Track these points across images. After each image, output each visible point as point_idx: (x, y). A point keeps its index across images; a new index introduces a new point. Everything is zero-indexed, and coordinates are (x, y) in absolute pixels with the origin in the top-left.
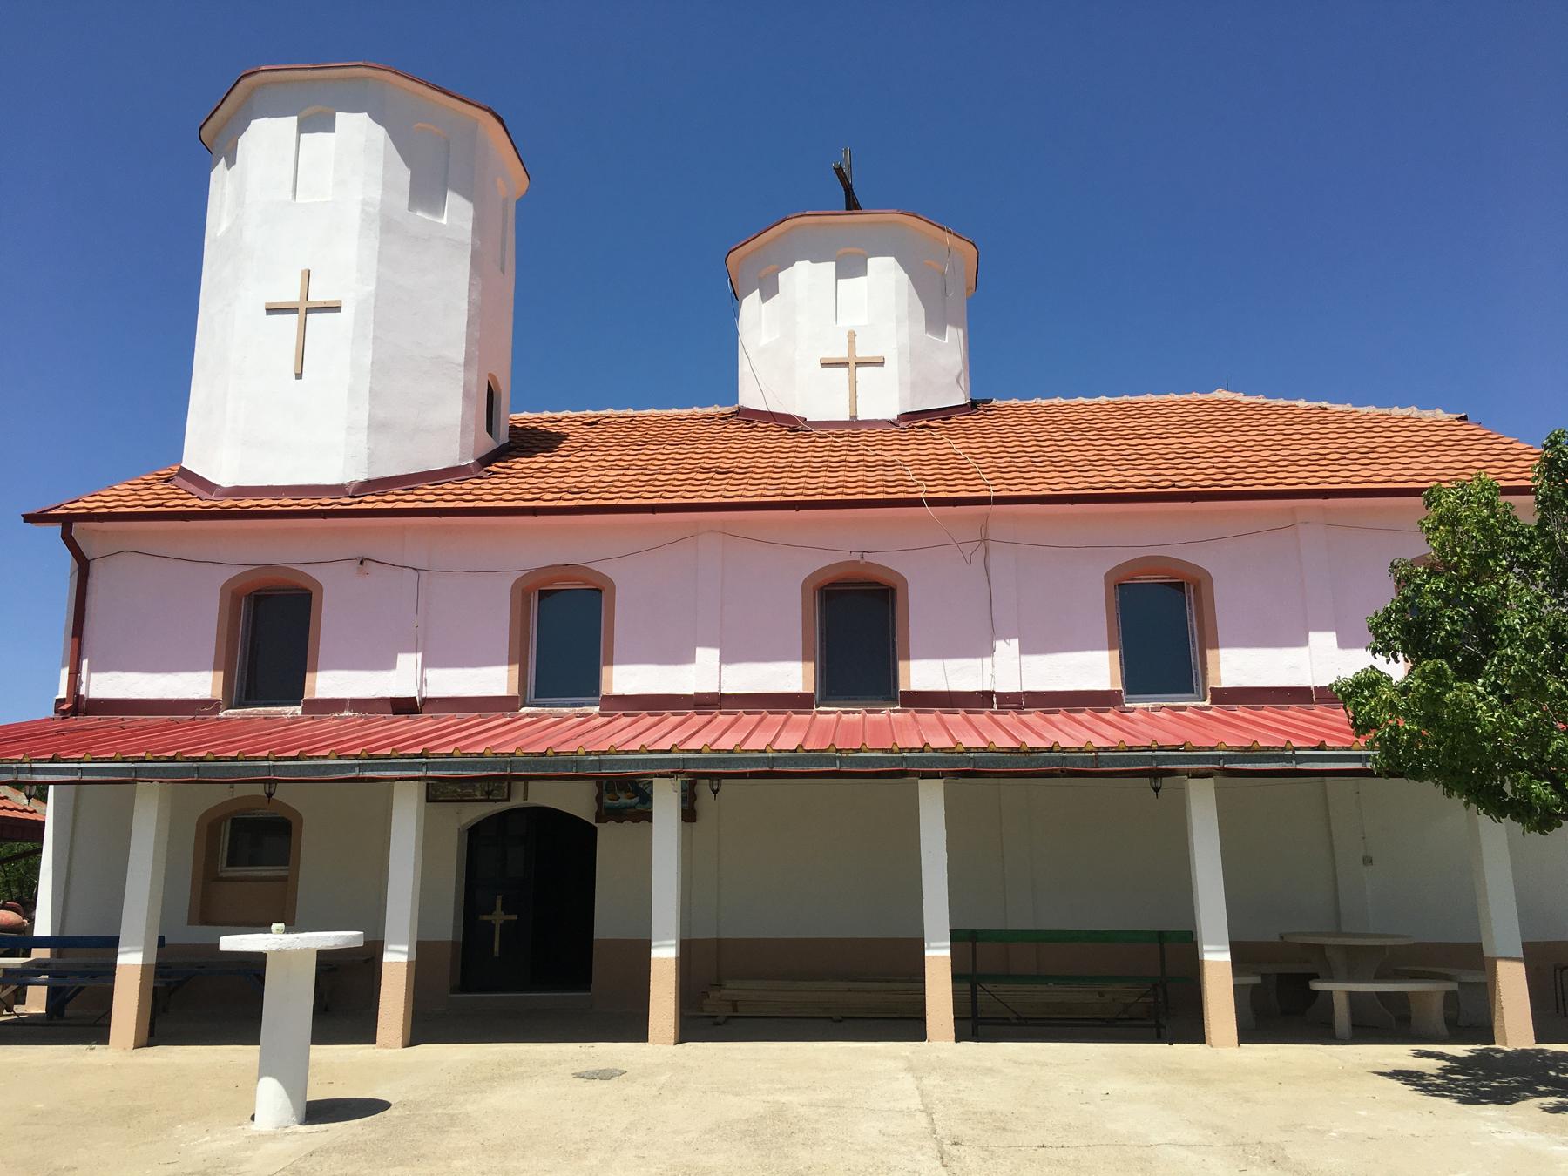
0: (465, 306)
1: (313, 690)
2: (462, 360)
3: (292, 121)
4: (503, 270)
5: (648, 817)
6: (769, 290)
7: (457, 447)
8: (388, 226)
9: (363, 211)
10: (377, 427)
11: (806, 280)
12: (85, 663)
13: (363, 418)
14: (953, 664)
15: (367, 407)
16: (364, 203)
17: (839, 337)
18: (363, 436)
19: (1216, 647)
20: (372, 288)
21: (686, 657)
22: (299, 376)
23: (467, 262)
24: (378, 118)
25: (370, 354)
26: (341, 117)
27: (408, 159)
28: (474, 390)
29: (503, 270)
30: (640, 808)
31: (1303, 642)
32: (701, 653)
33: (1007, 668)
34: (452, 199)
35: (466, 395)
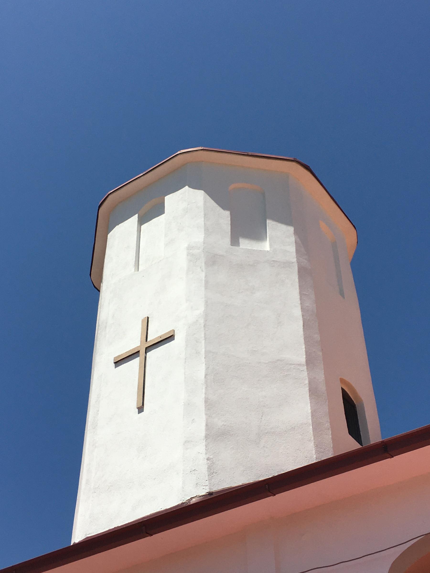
0: (298, 312)
2: (303, 359)
3: (135, 219)
4: (342, 294)
7: (311, 445)
8: (212, 260)
9: (188, 254)
10: (215, 435)
13: (200, 429)
15: (204, 417)
16: (189, 248)
18: (201, 448)
20: (201, 309)
22: (141, 409)
23: (295, 277)
24: (195, 186)
25: (203, 367)
27: (223, 204)
28: (323, 388)
29: (342, 294)
34: (272, 227)
35: (313, 392)
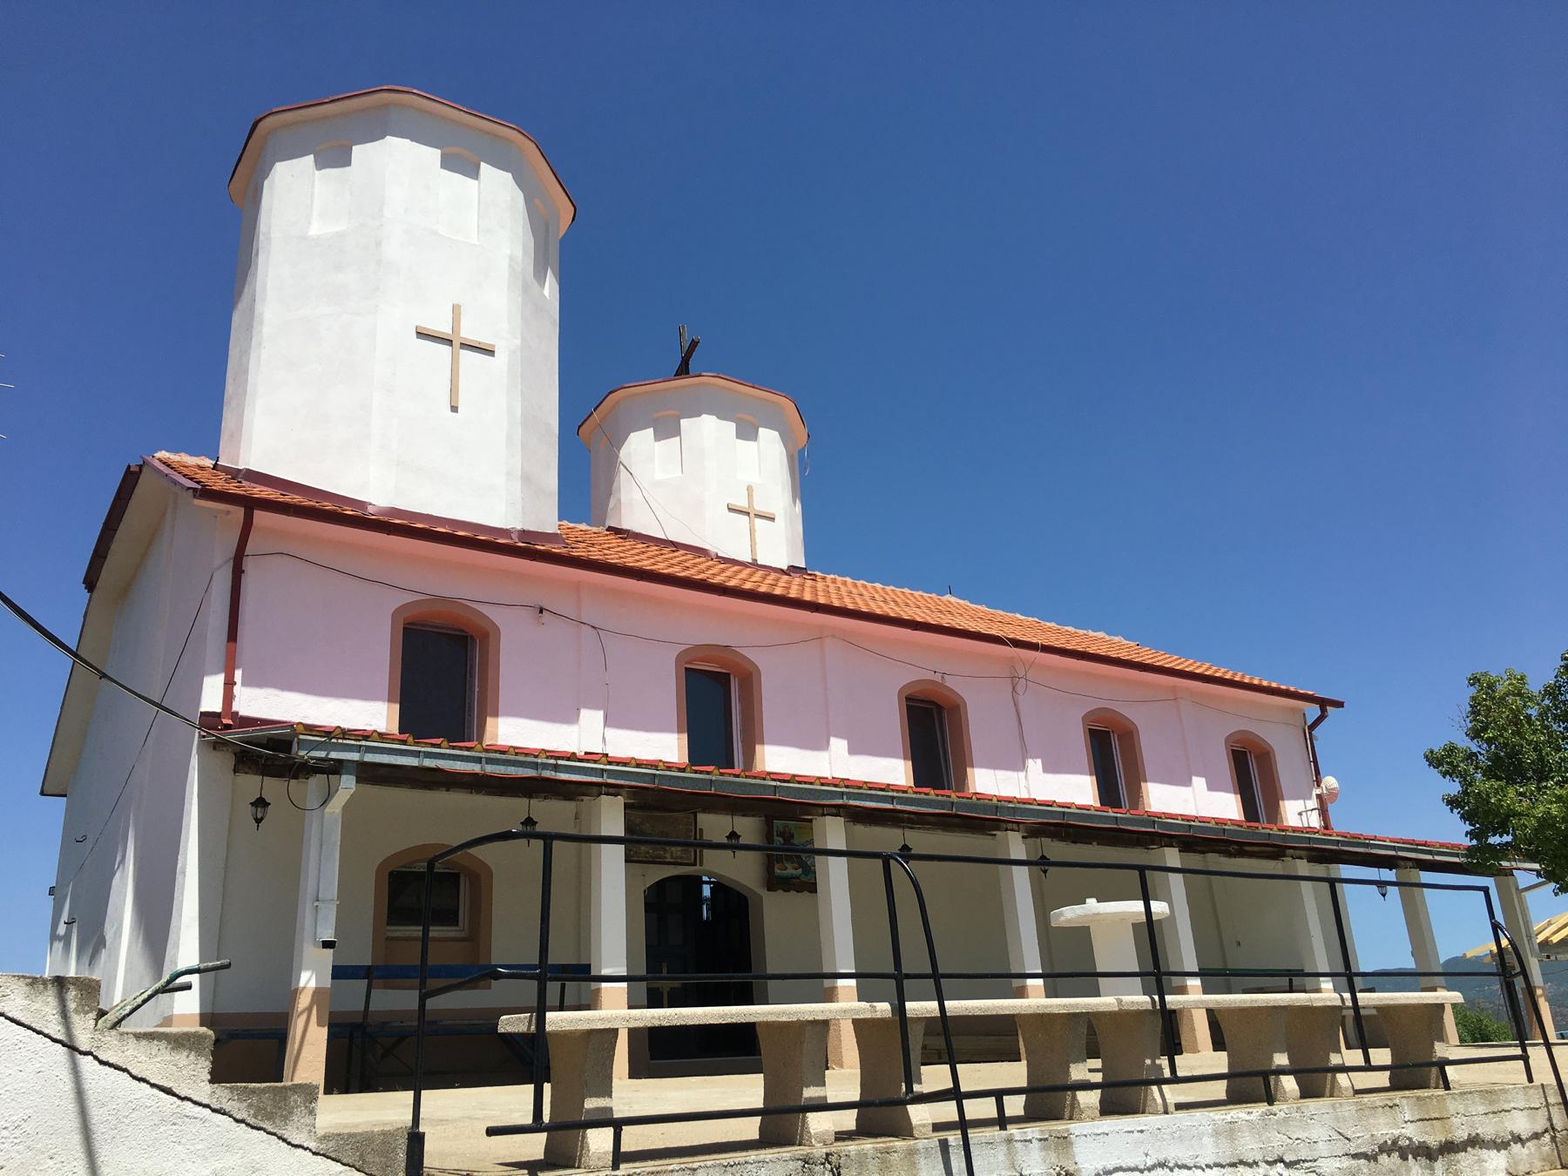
1: (496, 735)
5: (812, 888)
6: (667, 429)
11: (708, 432)
12: (238, 674)
14: (1001, 774)
17: (716, 484)
19: (496, 715)
20: (518, 342)
21: (571, 717)
24: (519, 181)
26: (485, 168)
30: (804, 878)
31: (1187, 782)
32: (1195, 779)
33: (585, 735)
